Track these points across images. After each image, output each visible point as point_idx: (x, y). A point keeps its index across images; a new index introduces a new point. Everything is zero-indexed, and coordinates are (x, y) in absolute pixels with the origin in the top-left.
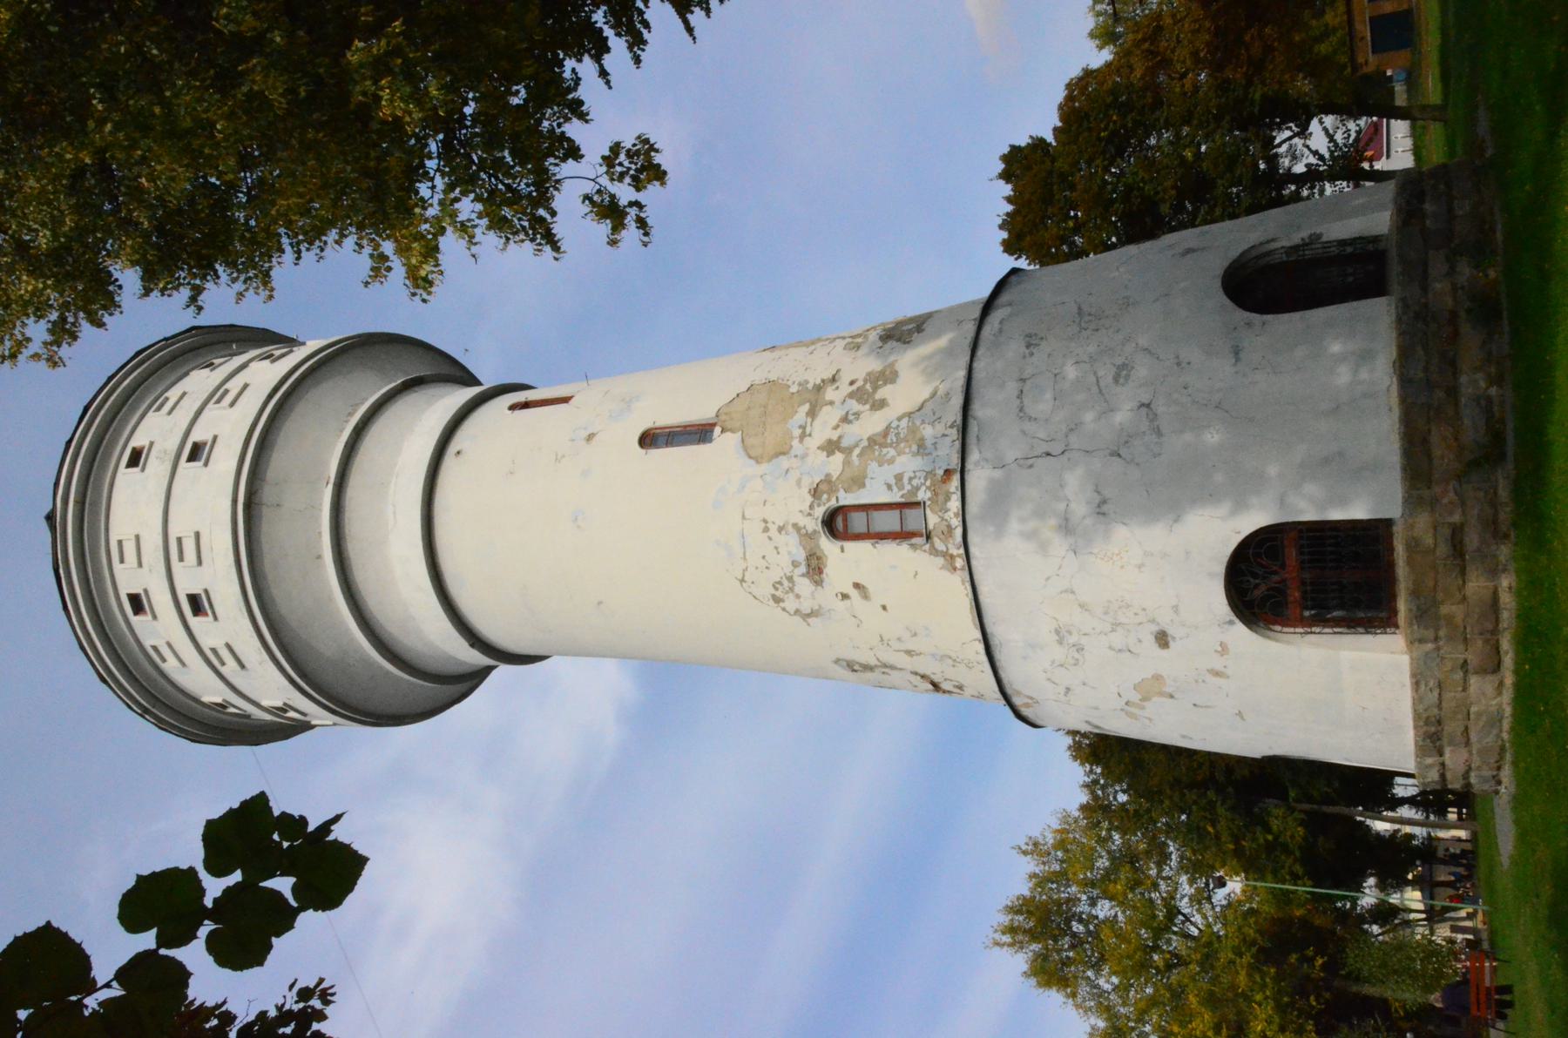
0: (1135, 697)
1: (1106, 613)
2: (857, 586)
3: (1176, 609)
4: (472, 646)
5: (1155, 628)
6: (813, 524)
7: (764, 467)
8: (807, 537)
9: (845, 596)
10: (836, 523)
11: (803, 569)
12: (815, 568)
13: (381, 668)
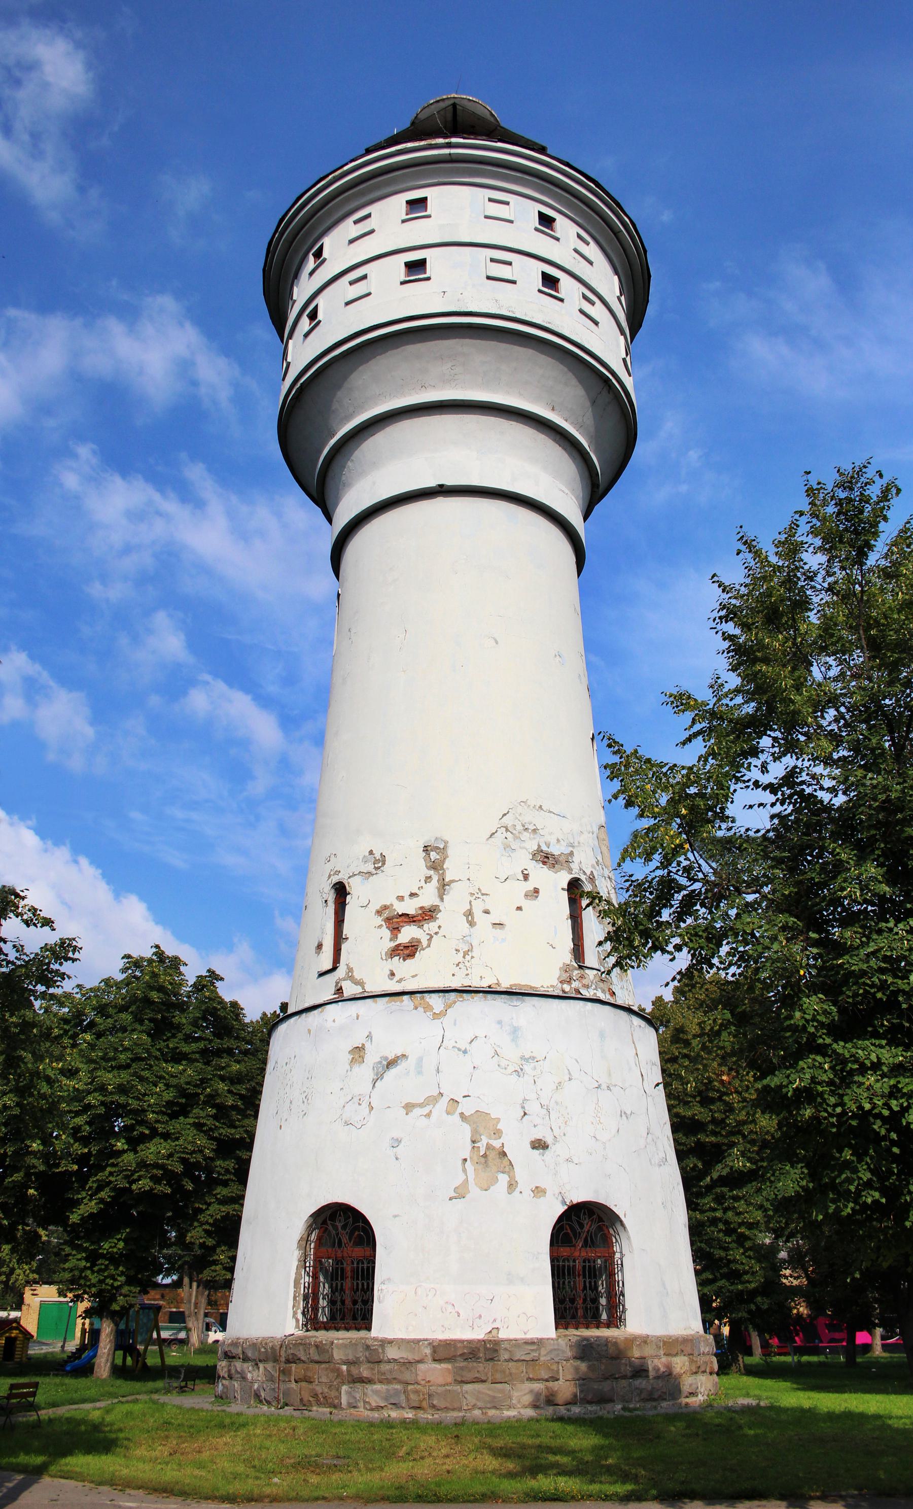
1: (557, 1103)
5: (549, 1140)
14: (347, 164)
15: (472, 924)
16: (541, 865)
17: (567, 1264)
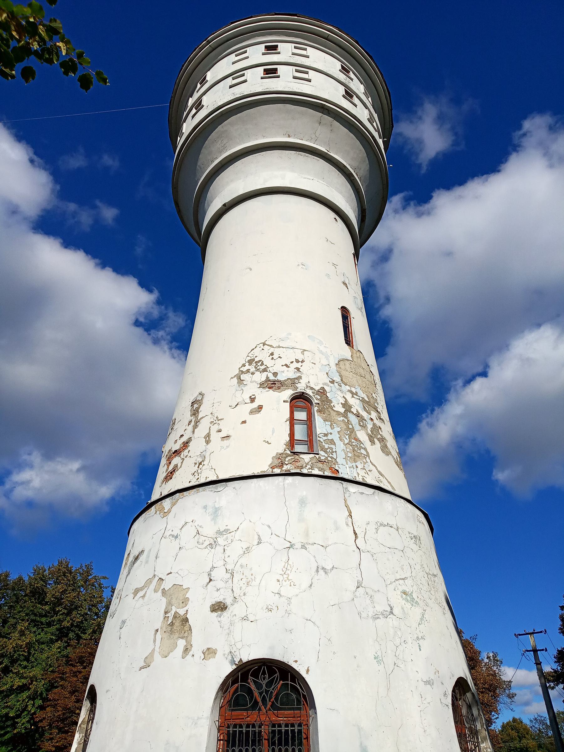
0: (167, 585)
1: (242, 566)
2: (260, 407)
3: (245, 619)
4: (224, 205)
5: (228, 602)
6: (301, 387)
7: (334, 368)
8: (293, 382)
9: (252, 400)
10: (300, 400)
11: (272, 377)
12: (273, 384)
13: (209, 166)
14: (183, 66)
15: (208, 442)
16: (267, 389)
17: (290, 728)
